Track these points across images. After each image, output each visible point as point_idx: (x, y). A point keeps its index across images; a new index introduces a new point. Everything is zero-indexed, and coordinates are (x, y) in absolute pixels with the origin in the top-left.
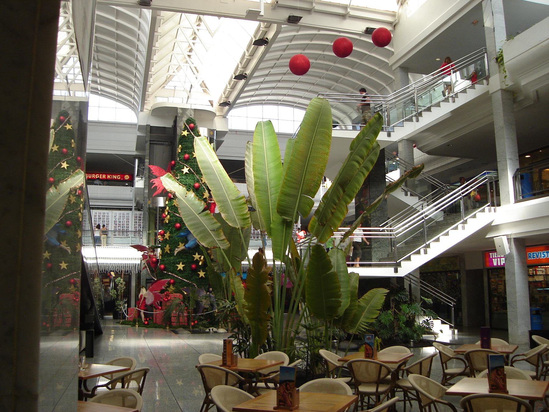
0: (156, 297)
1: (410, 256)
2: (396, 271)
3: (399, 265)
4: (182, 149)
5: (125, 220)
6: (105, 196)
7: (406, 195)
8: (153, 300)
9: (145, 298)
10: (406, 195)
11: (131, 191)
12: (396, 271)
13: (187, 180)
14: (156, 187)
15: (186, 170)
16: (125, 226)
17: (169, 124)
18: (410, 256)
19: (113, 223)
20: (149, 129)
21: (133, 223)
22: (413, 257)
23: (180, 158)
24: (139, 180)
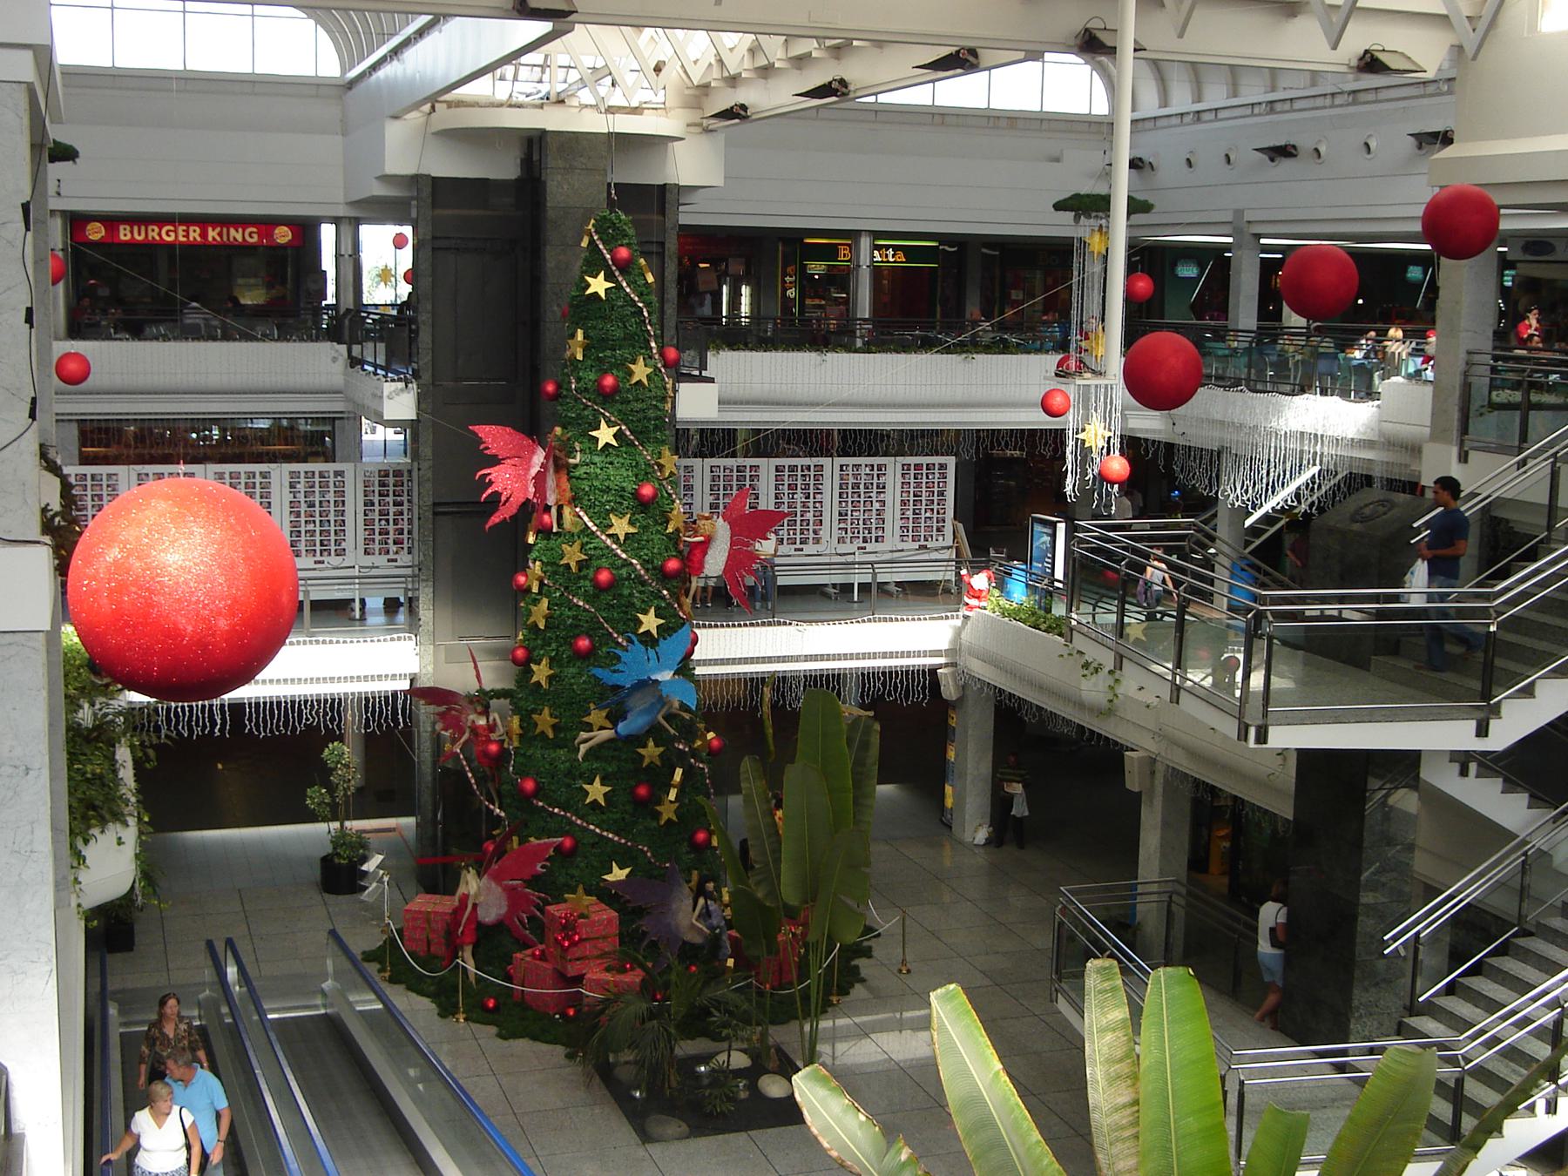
0: (512, 895)
1: (1532, 683)
2: (1482, 731)
3: (1495, 711)
4: (586, 349)
5: (331, 497)
6: (237, 381)
7: (1464, 772)
8: (504, 910)
9: (475, 906)
10: (1464, 772)
11: (334, 360)
12: (1482, 731)
13: (611, 471)
14: (497, 494)
15: (605, 435)
16: (332, 518)
17: (504, 168)
18: (1532, 683)
19: (287, 509)
20: (427, 191)
21: (361, 508)
22: (1539, 688)
23: (579, 380)
24: (398, 392)
